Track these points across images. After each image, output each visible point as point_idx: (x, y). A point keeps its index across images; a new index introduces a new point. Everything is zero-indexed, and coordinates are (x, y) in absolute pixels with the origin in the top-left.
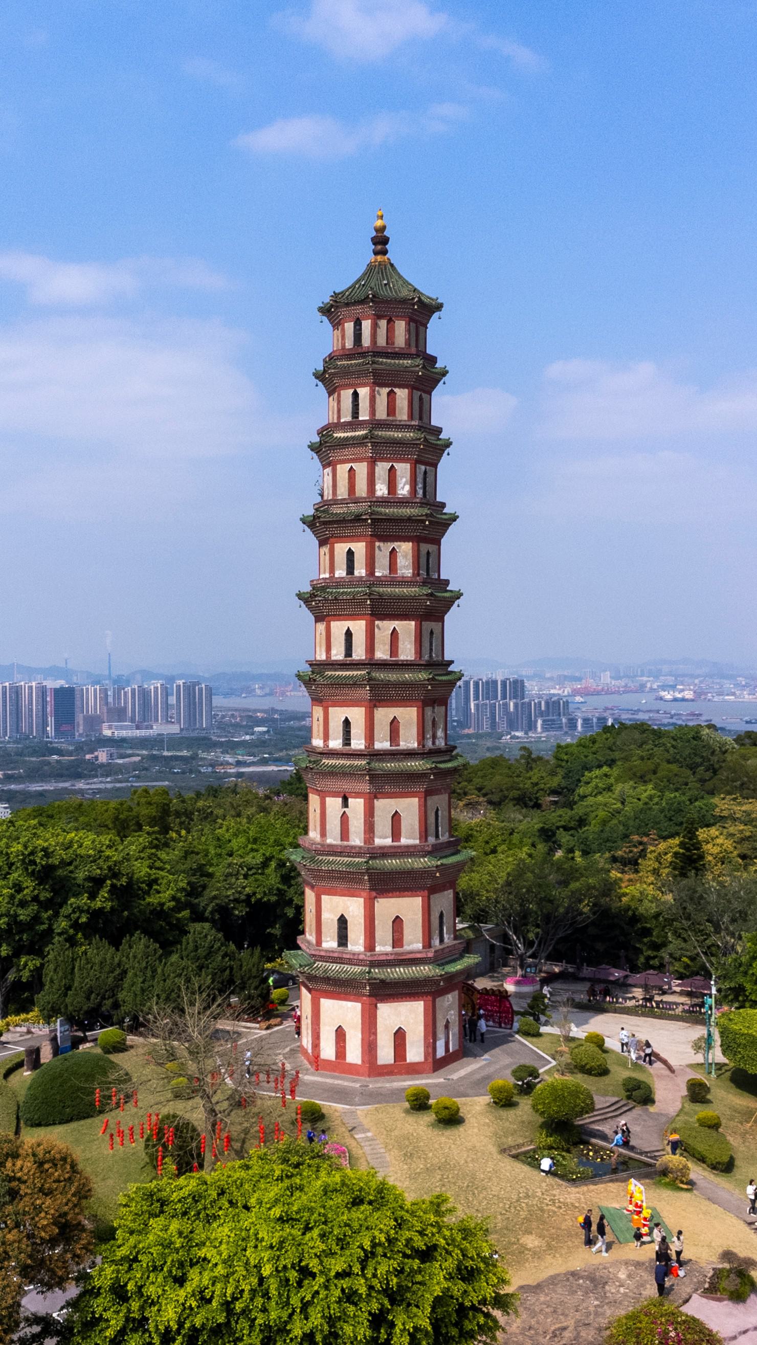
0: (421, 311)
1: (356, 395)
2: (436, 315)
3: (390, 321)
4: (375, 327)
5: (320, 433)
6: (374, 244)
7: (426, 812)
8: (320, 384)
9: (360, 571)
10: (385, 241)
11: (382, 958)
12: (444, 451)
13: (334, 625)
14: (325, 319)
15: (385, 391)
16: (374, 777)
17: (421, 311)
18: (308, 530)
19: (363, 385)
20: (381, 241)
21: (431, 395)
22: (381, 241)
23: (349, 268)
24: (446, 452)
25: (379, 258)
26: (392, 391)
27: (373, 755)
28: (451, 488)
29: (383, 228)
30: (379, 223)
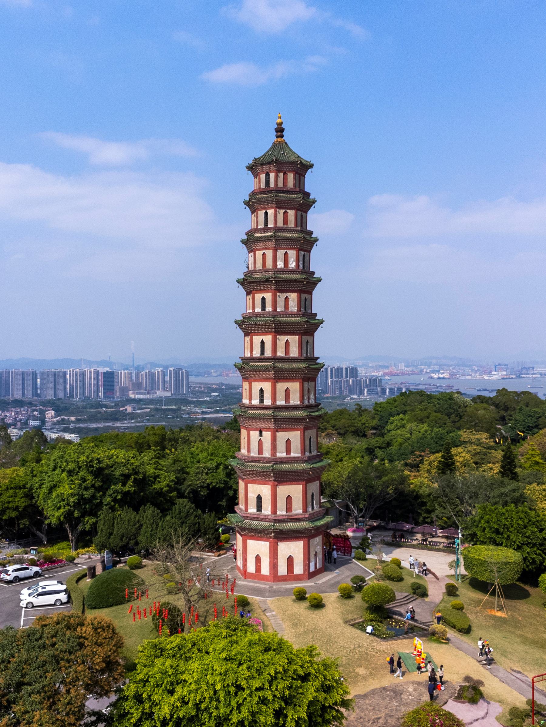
0: (302, 168)
1: (266, 214)
2: (310, 170)
3: (285, 174)
6: (277, 132)
7: (300, 301)
10: (282, 130)
11: (282, 518)
15: (282, 211)
16: (276, 420)
17: (302, 168)
19: (271, 208)
20: (280, 130)
22: (280, 130)
25: (279, 139)
26: (286, 252)
27: (276, 408)
29: (281, 123)
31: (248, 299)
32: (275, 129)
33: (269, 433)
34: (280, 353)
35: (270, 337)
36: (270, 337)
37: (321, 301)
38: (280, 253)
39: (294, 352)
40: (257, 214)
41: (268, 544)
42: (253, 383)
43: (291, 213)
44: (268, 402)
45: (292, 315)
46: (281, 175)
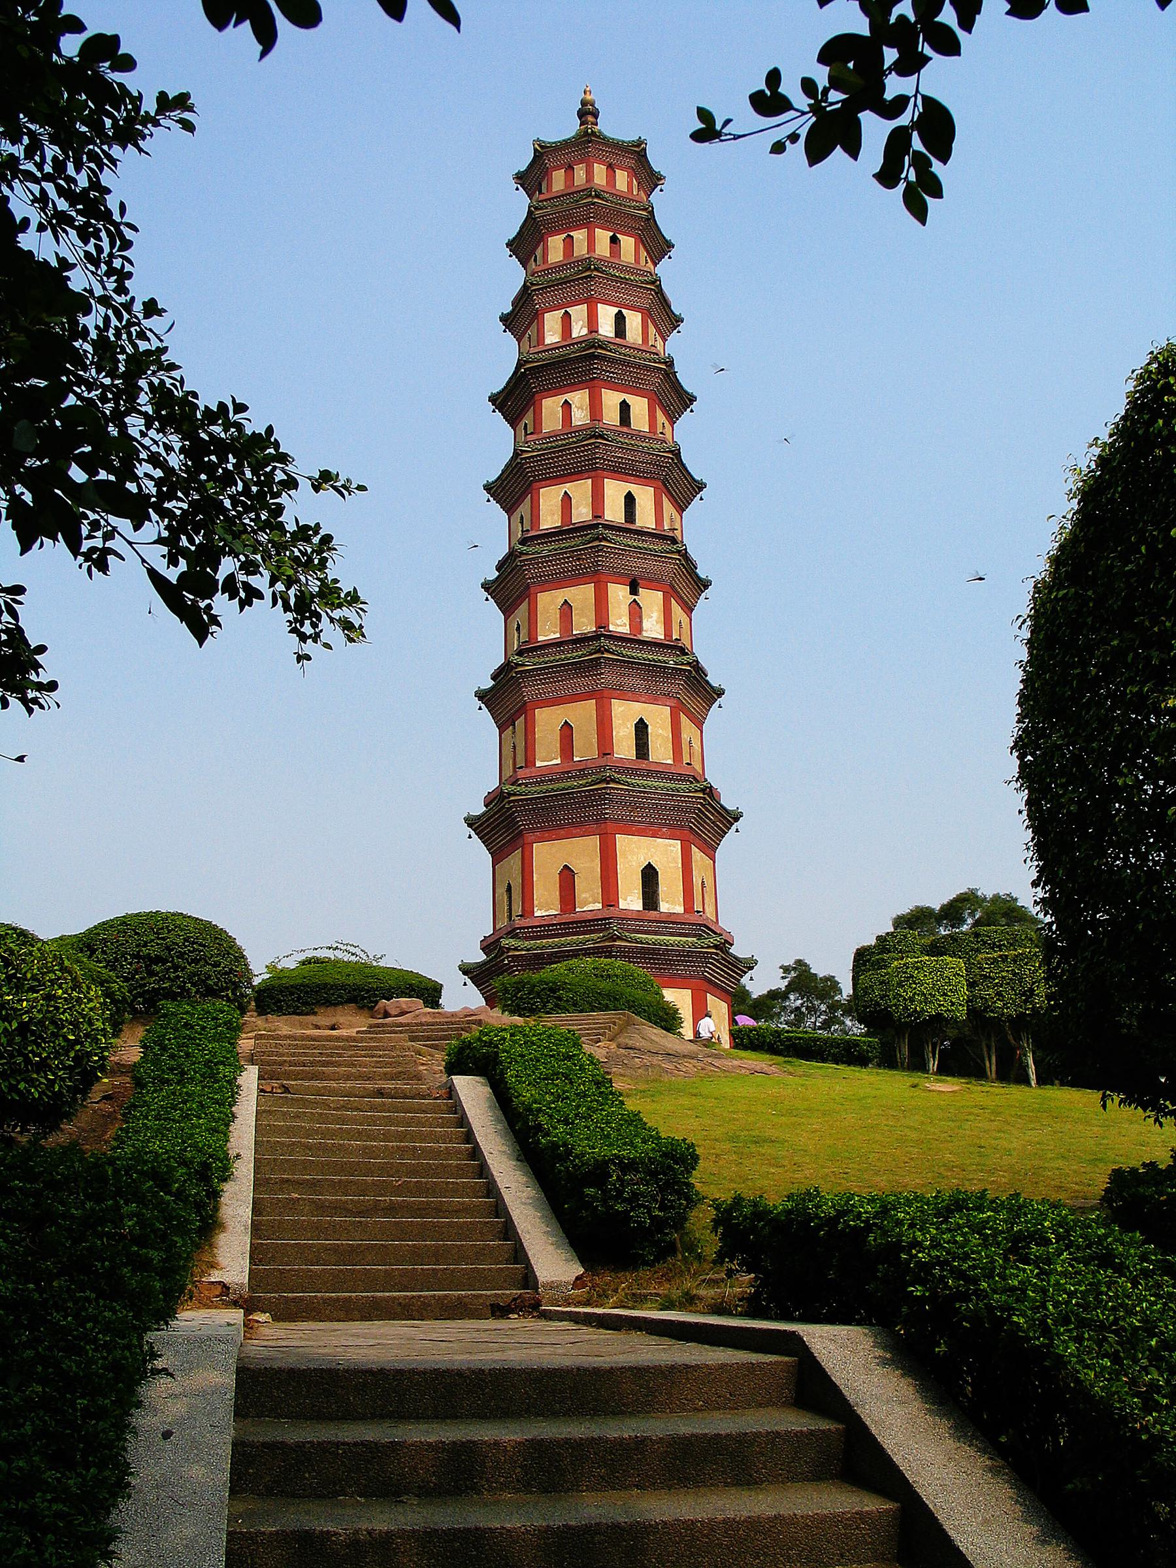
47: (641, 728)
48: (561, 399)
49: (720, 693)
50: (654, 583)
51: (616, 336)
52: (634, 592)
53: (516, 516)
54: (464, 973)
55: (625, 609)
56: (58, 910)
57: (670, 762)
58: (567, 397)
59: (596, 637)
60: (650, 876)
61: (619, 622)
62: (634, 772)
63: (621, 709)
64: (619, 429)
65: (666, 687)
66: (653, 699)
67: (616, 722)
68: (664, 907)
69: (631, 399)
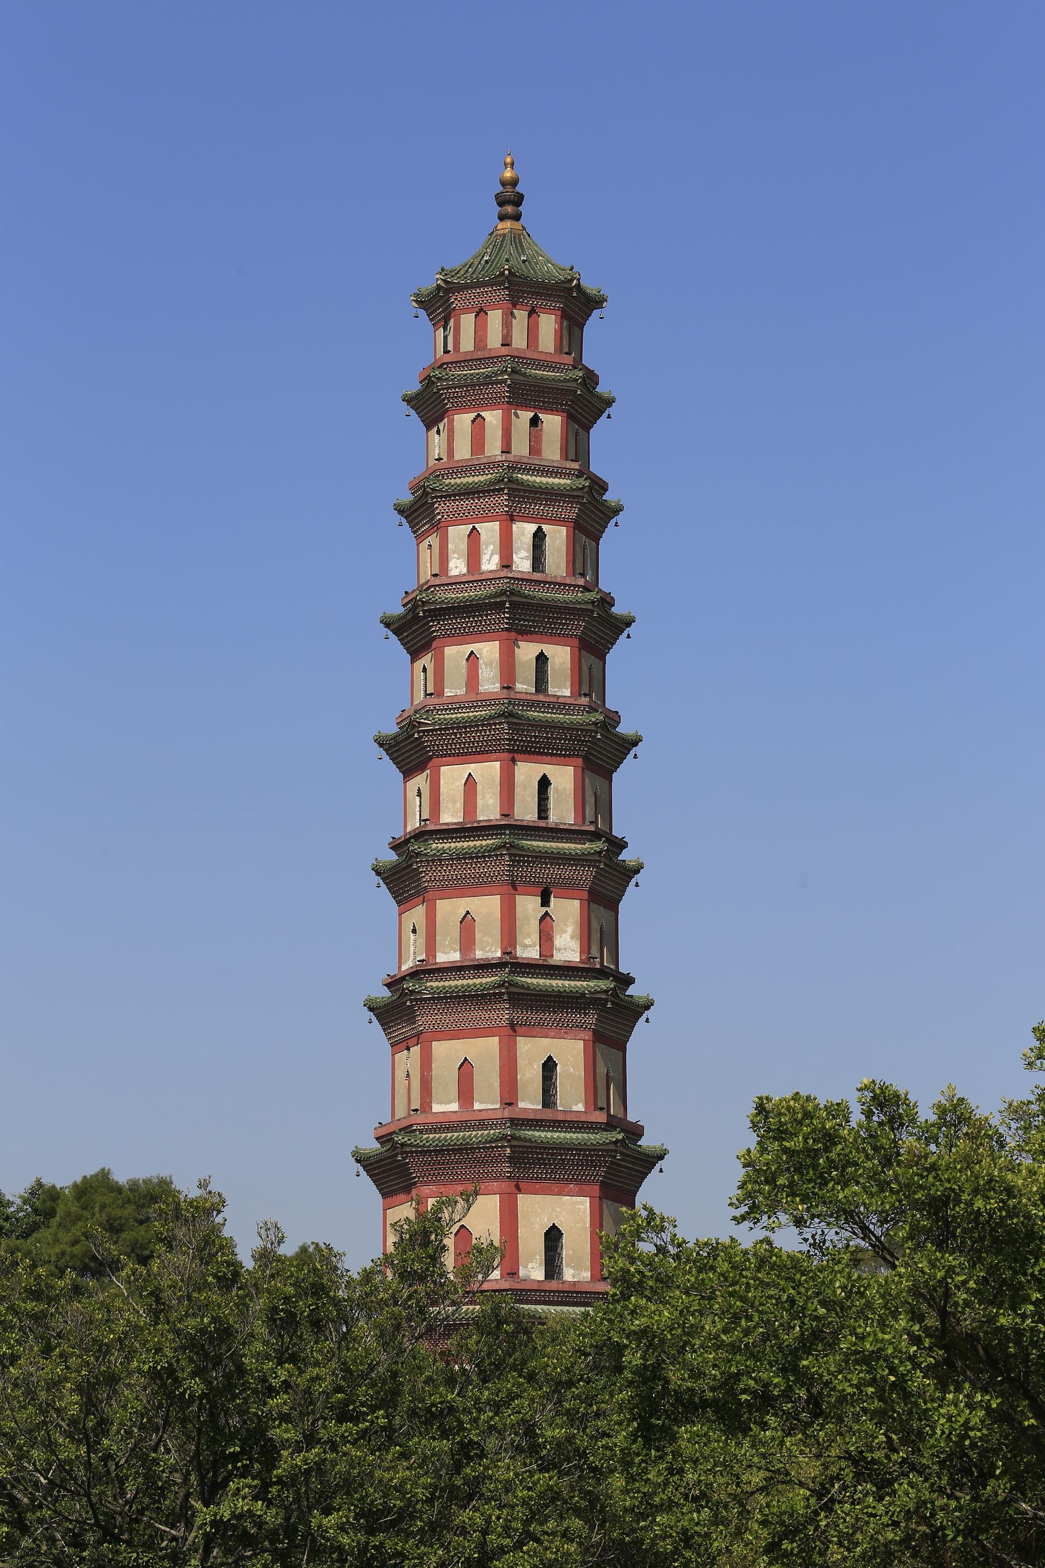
0: (576, 305)
1: (474, 533)
2: (596, 313)
3: (532, 312)
4: (507, 326)
5: (414, 489)
6: (501, 204)
7: (580, 669)
8: (413, 412)
9: (490, 562)
10: (518, 200)
11: (523, 697)
12: (631, 878)
13: (440, 1048)
14: (422, 313)
15: (526, 415)
16: (519, 857)
17: (576, 305)
18: (394, 638)
19: (490, 406)
20: (510, 201)
21: (624, 1051)
22: (510, 201)
23: (465, 238)
24: (632, 753)
25: (508, 224)
26: (540, 529)
27: (512, 964)
28: (623, 569)
29: (514, 182)
30: (508, 174)
31: (412, 793)
32: (497, 196)
33: (498, 313)
34: (526, 811)
35: (494, 768)
36: (494, 768)
37: (764, 1095)
38: (523, 531)
39: (563, 812)
40: (451, 422)
41: (497, 898)
42: (439, 903)
43: (553, 423)
44: (488, 949)
45: (558, 705)
46: (521, 315)
47: (549, 1067)
48: (468, 648)
49: (628, 622)
50: (568, 888)
51: (540, 818)
52: (545, 903)
53: (419, 664)
54: (358, 1161)
55: (534, 925)
56: (15, 1190)
57: (580, 1107)
58: (472, 768)
59: (500, 965)
60: (553, 1237)
61: (528, 941)
62: (533, 705)
63: (526, 1048)
64: (534, 698)
65: (578, 1018)
66: (562, 1030)
67: (521, 1063)
68: (569, 1275)
69: (549, 650)
